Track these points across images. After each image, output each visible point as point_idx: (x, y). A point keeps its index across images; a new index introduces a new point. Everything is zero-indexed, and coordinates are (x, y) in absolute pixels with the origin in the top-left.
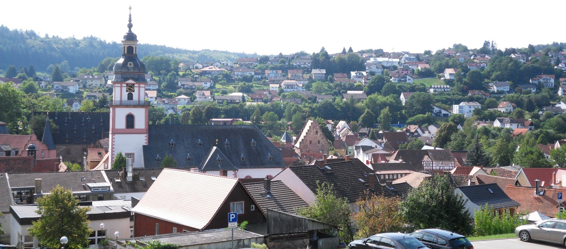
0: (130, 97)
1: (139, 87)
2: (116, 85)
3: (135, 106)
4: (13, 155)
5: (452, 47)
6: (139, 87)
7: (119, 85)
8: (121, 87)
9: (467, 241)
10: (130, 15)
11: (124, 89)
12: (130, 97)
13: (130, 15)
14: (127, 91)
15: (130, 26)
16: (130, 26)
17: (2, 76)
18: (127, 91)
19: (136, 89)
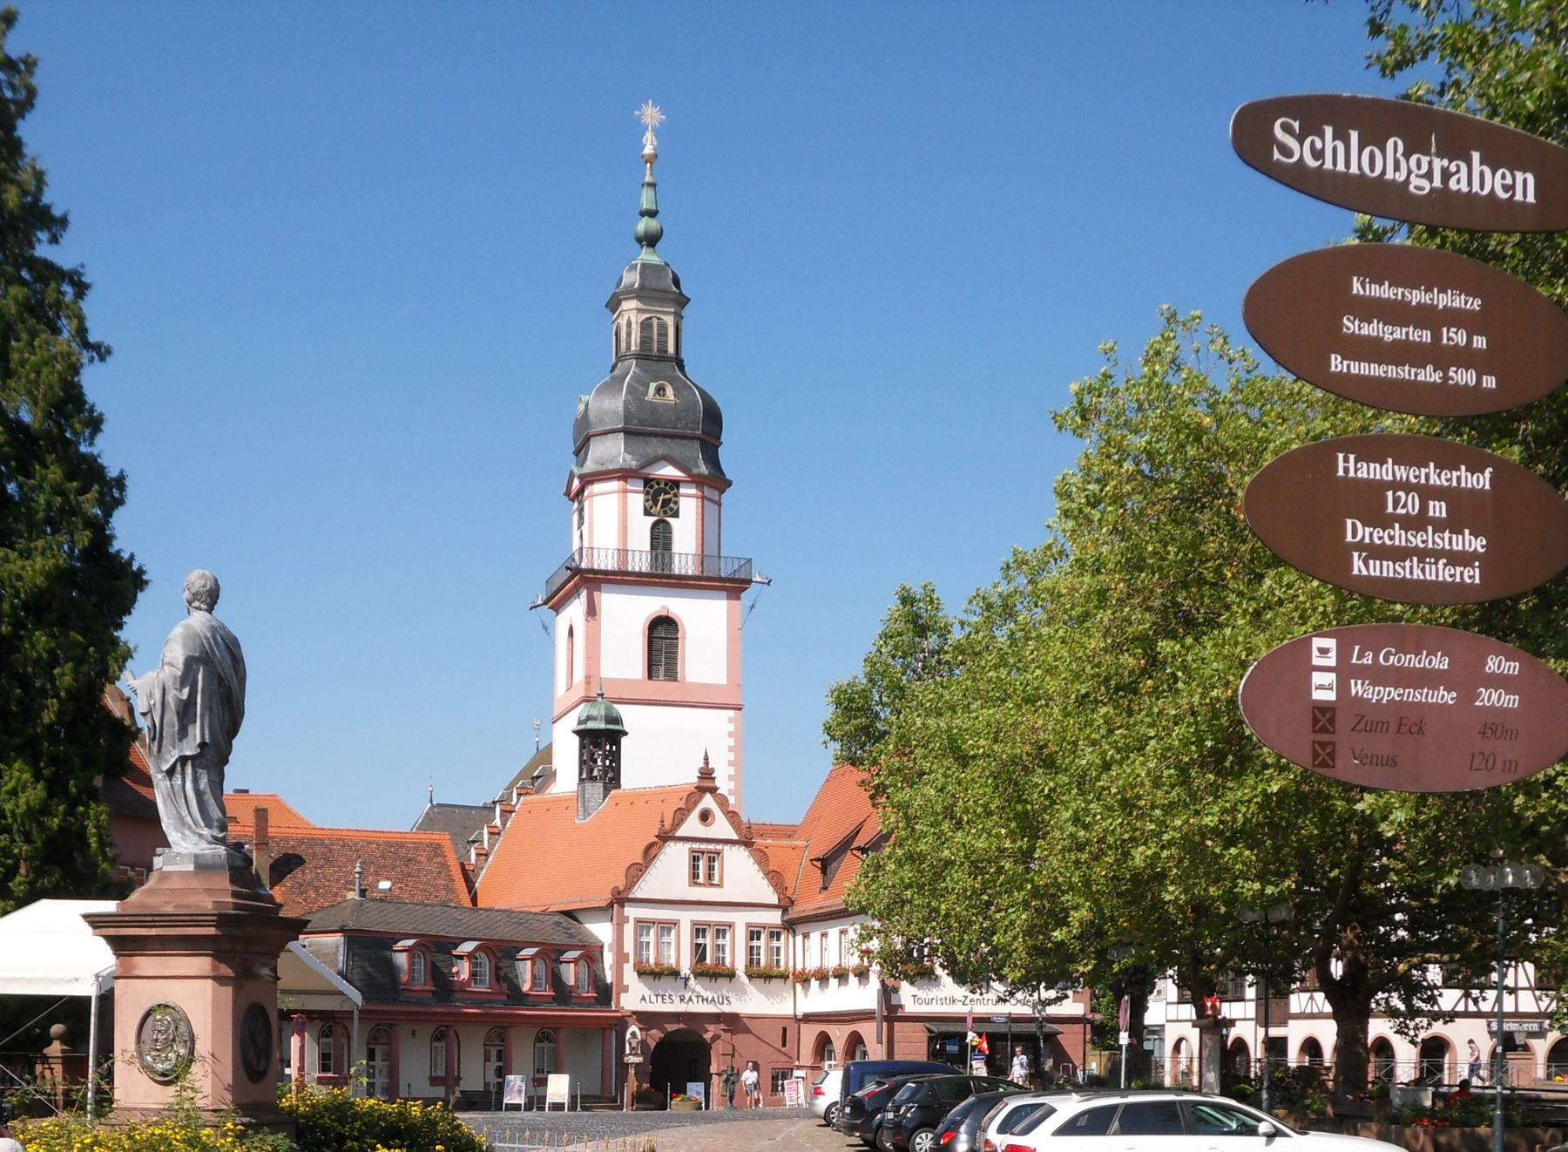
0: (661, 538)
1: (623, 552)
12: (661, 538)
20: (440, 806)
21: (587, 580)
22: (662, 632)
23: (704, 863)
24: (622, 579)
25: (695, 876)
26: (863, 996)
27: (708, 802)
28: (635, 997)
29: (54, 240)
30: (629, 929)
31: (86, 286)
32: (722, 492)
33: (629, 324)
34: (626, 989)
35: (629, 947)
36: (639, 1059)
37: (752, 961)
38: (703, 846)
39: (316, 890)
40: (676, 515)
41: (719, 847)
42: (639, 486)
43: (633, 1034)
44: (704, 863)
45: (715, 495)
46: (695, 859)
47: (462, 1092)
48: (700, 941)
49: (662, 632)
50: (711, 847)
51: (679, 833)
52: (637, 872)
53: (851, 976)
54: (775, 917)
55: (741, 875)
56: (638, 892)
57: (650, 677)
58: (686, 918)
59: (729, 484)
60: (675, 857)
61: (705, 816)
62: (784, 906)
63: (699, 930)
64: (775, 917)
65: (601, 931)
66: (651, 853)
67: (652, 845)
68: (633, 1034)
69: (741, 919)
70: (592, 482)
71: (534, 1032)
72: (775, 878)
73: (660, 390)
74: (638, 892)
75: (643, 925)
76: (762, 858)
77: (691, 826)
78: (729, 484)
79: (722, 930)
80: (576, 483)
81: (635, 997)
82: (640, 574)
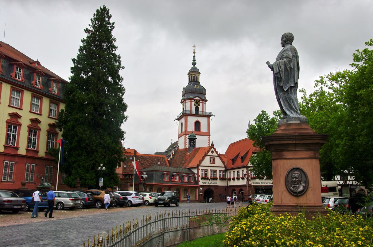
0: (197, 109)
1: (191, 111)
2: (187, 101)
3: (201, 116)
4: (40, 195)
5: (117, 53)
6: (191, 111)
7: (189, 101)
8: (191, 102)
9: (44, 211)
10: (194, 57)
11: (193, 103)
12: (197, 109)
13: (194, 57)
14: (195, 105)
15: (194, 64)
16: (194, 64)
17: (1, 231)
18: (195, 105)
19: (201, 104)
20: (157, 152)
21: (185, 115)
22: (197, 124)
23: (212, 160)
24: (191, 115)
25: (210, 162)
26: (243, 182)
27: (212, 149)
28: (201, 182)
29: (115, 50)
30: (200, 171)
31: (120, 57)
32: (206, 102)
33: (191, 76)
34: (200, 181)
35: (200, 174)
36: (202, 194)
37: (211, 176)
38: (211, 157)
39: (144, 165)
40: (199, 105)
41: (214, 157)
42: (193, 101)
43: (201, 189)
44: (212, 160)
45: (205, 102)
46: (211, 159)
47: (127, 197)
48: (220, 174)
49: (197, 124)
50: (213, 157)
51: (208, 155)
52: (201, 161)
53: (231, 180)
54: (223, 169)
55: (218, 162)
56: (201, 165)
57: (195, 131)
58: (209, 169)
59: (207, 101)
60: (207, 159)
61: (212, 152)
62: (225, 167)
63: (211, 171)
64: (223, 169)
65: (195, 171)
66: (203, 158)
67: (204, 157)
68: (201, 189)
69: (218, 169)
70: (186, 100)
71: (184, 188)
72: (224, 163)
73: (197, 86)
74: (201, 165)
75: (202, 170)
76: (221, 159)
77: (210, 153)
78: (207, 101)
79: (215, 171)
80: (183, 100)
81: (201, 182)
82: (194, 114)
